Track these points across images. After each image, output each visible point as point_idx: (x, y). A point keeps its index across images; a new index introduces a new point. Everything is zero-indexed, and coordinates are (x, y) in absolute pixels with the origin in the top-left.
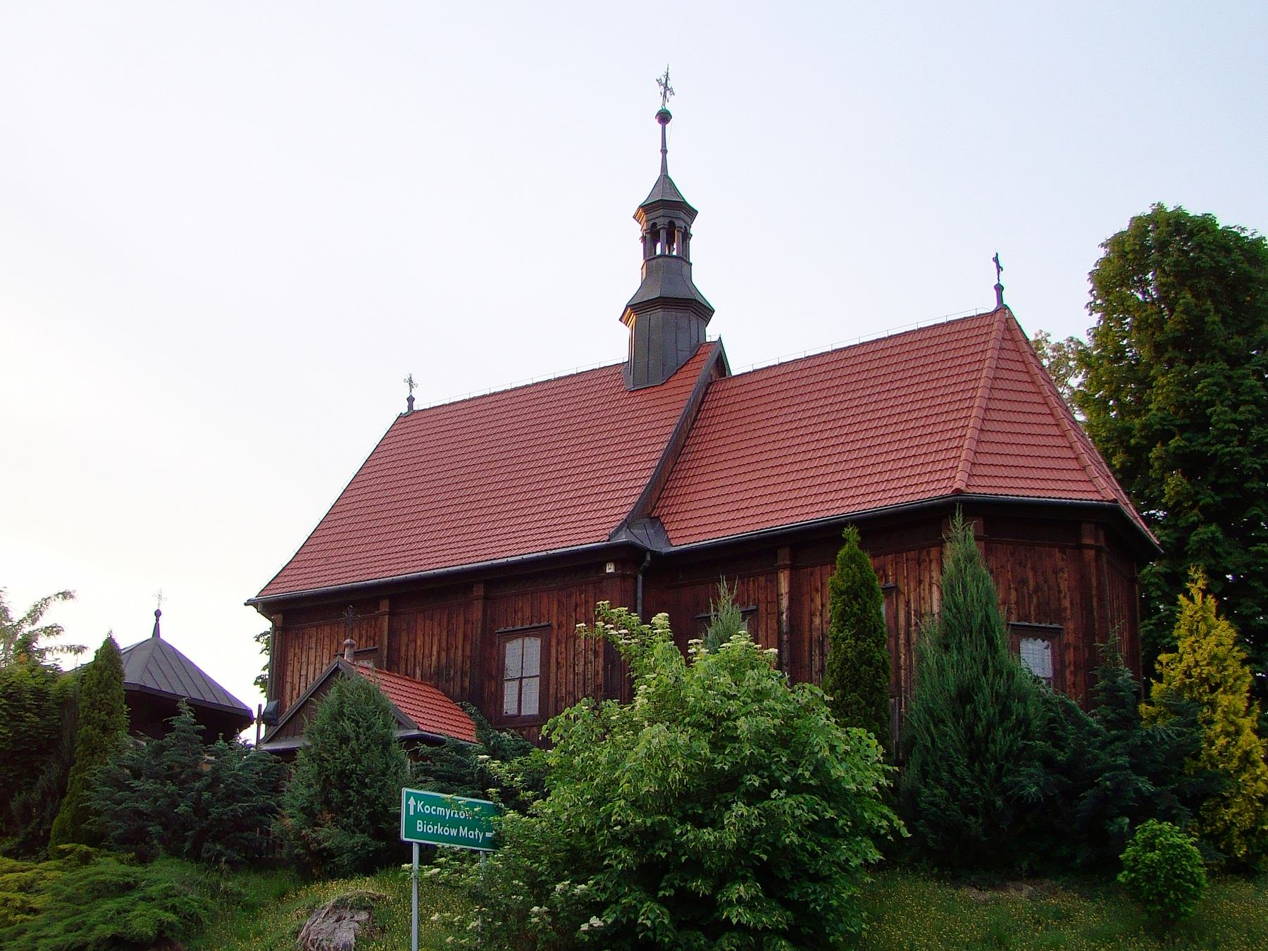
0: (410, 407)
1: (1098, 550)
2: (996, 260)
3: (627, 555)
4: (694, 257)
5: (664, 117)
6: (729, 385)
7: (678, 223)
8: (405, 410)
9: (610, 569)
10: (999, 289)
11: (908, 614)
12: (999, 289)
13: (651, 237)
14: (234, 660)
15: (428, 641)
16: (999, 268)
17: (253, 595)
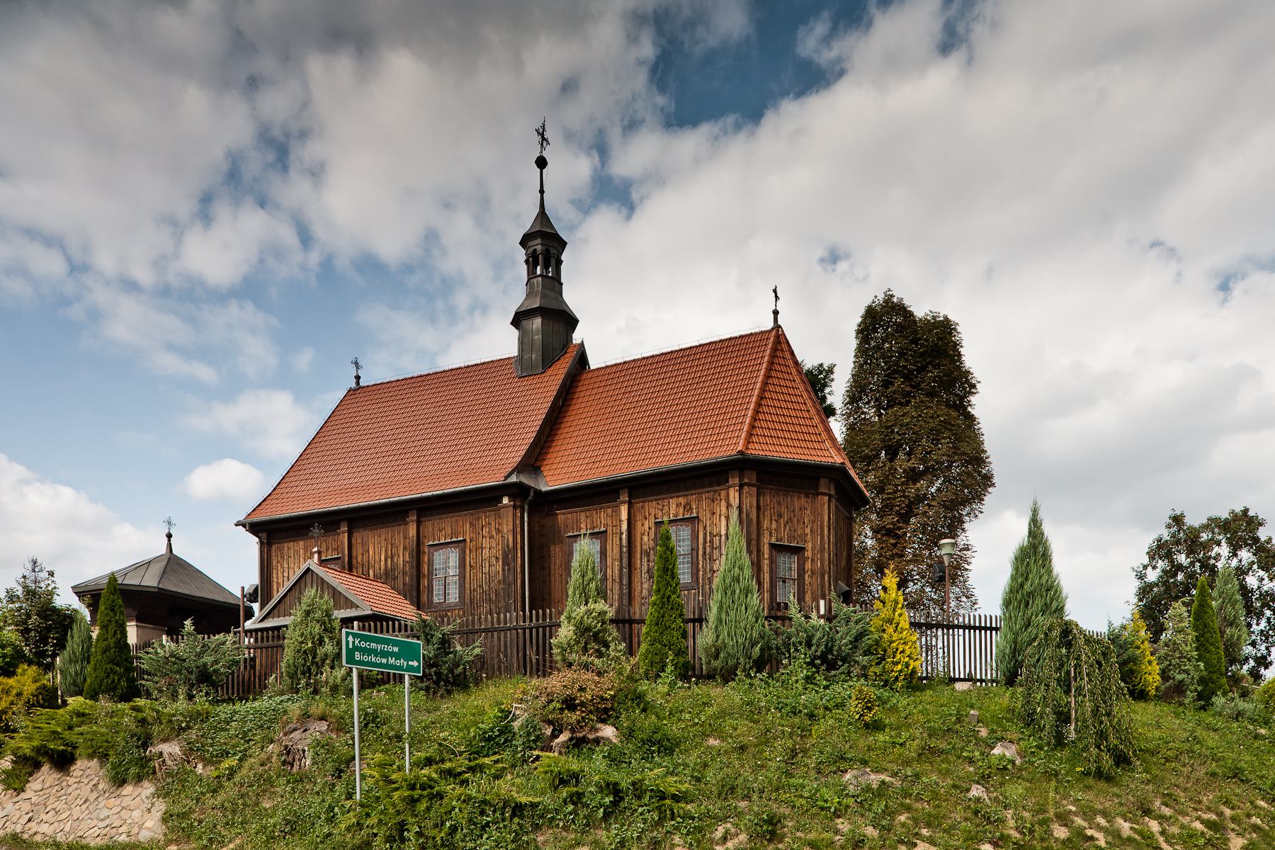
0: (358, 383)
1: (830, 496)
2: (775, 291)
3: (517, 492)
6: (590, 375)
7: (553, 251)
8: (353, 385)
9: (505, 500)
10: (776, 313)
11: (705, 534)
12: (776, 313)
13: (532, 261)
14: (232, 566)
15: (378, 547)
16: (777, 297)
17: (241, 518)
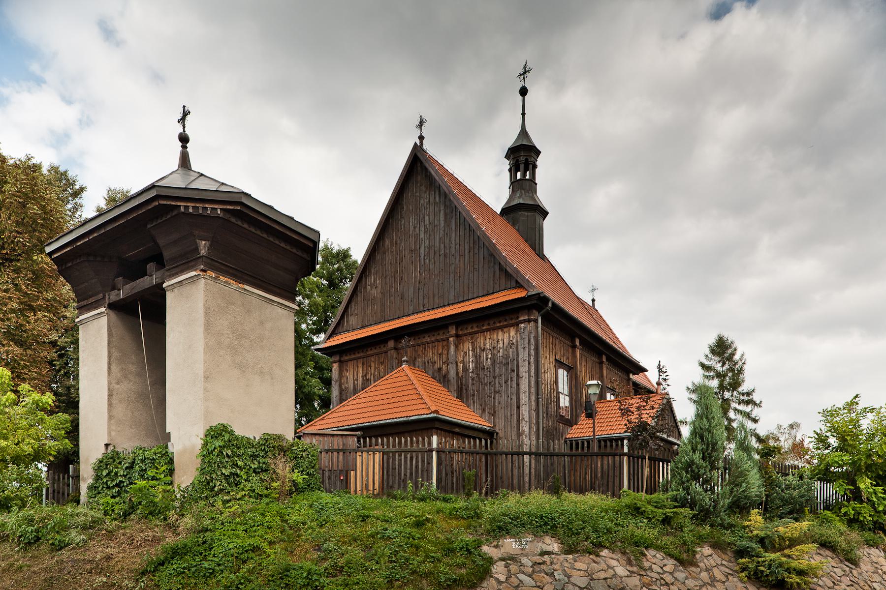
4: (538, 180)
5: (524, 92)
